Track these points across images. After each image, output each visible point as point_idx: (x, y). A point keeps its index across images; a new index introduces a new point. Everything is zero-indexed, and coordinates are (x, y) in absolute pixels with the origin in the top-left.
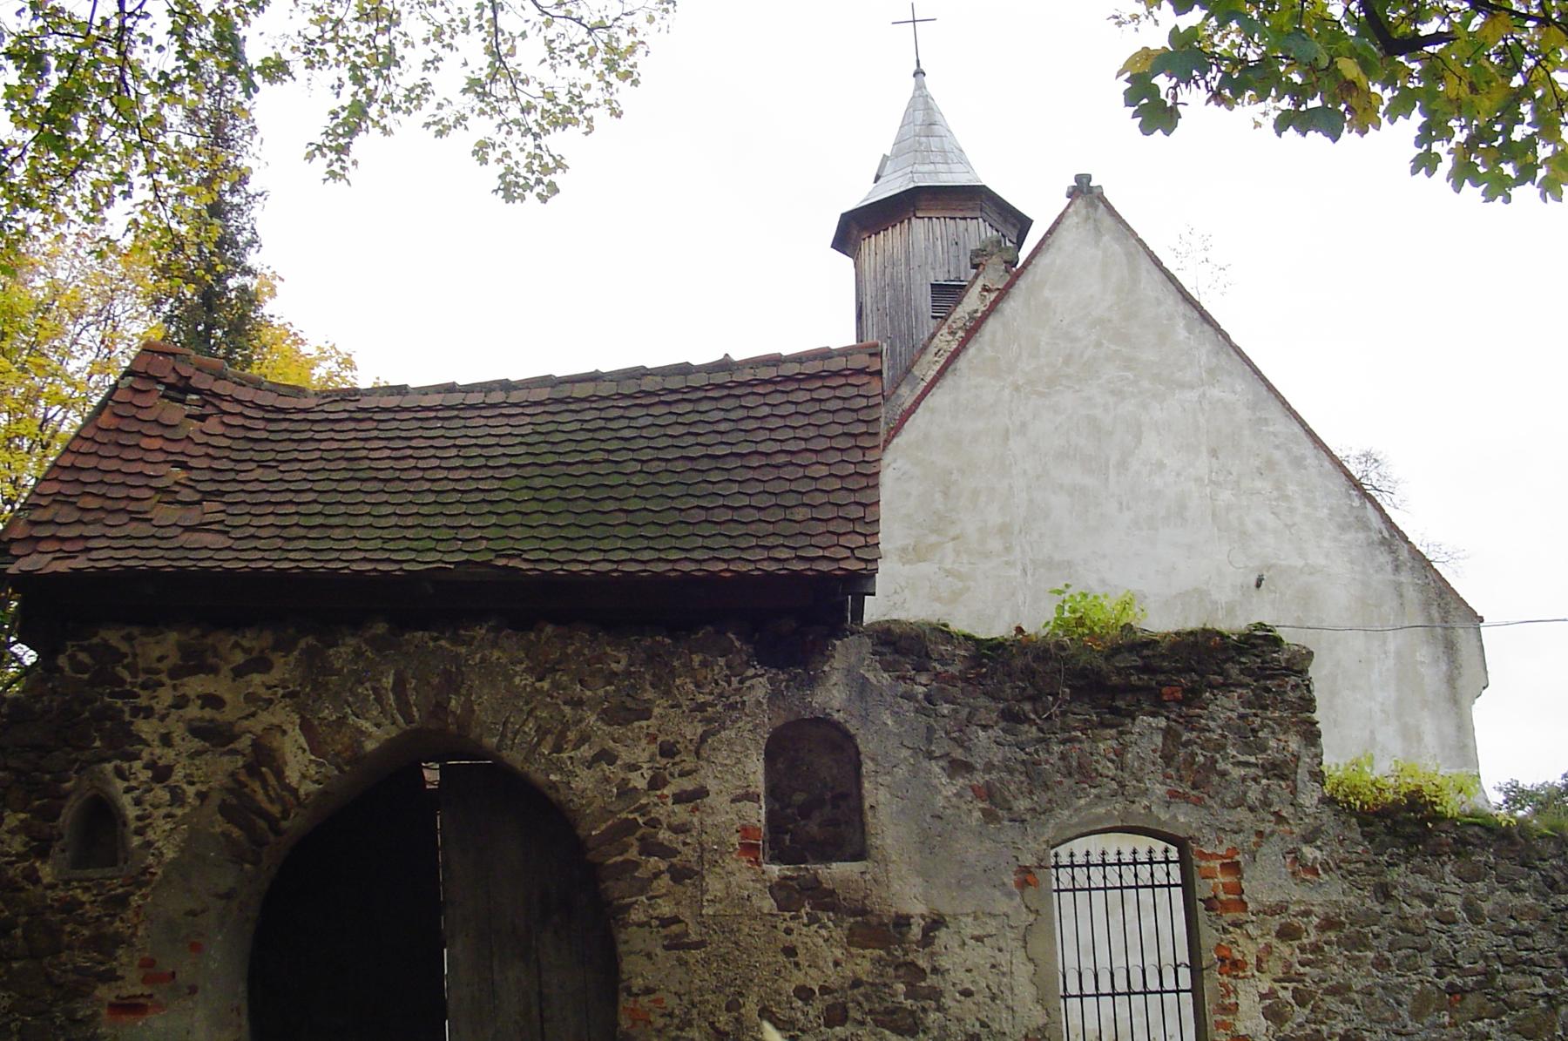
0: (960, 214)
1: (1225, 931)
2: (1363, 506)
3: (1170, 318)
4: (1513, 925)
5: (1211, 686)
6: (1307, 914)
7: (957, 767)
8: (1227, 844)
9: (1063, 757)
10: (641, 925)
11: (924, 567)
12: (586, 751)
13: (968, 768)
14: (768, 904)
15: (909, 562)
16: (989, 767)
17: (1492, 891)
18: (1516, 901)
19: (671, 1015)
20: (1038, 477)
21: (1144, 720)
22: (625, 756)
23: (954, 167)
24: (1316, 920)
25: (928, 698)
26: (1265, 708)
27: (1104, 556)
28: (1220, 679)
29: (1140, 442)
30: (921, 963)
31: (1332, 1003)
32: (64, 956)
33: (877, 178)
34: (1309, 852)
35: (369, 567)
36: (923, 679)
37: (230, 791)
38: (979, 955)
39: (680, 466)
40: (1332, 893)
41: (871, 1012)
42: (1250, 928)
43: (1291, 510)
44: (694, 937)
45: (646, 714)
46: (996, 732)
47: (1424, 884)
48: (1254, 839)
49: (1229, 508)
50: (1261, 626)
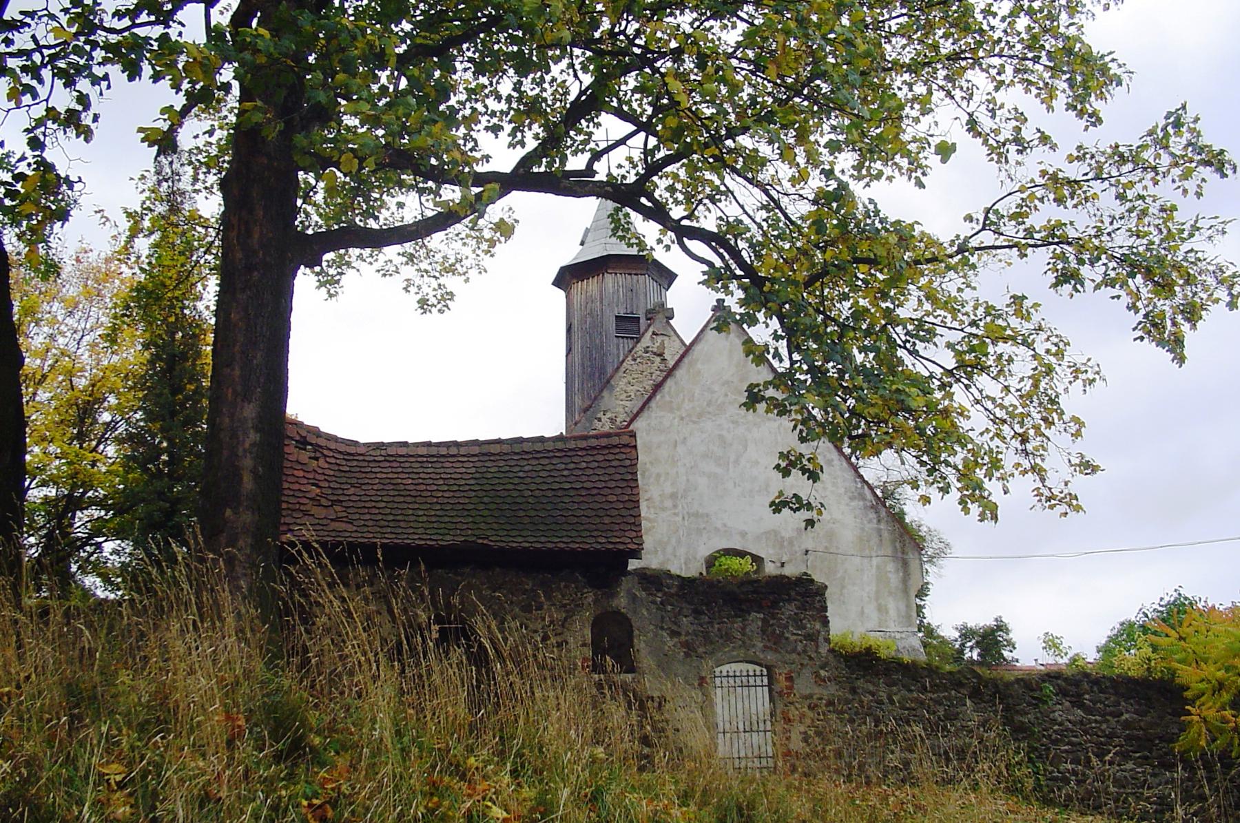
5: (783, 601)
6: (821, 699)
7: (674, 634)
9: (719, 630)
13: (678, 634)
16: (688, 634)
18: (909, 695)
25: (662, 603)
33: (582, 244)
34: (823, 673)
39: (550, 494)
46: (690, 619)
50: (805, 574)
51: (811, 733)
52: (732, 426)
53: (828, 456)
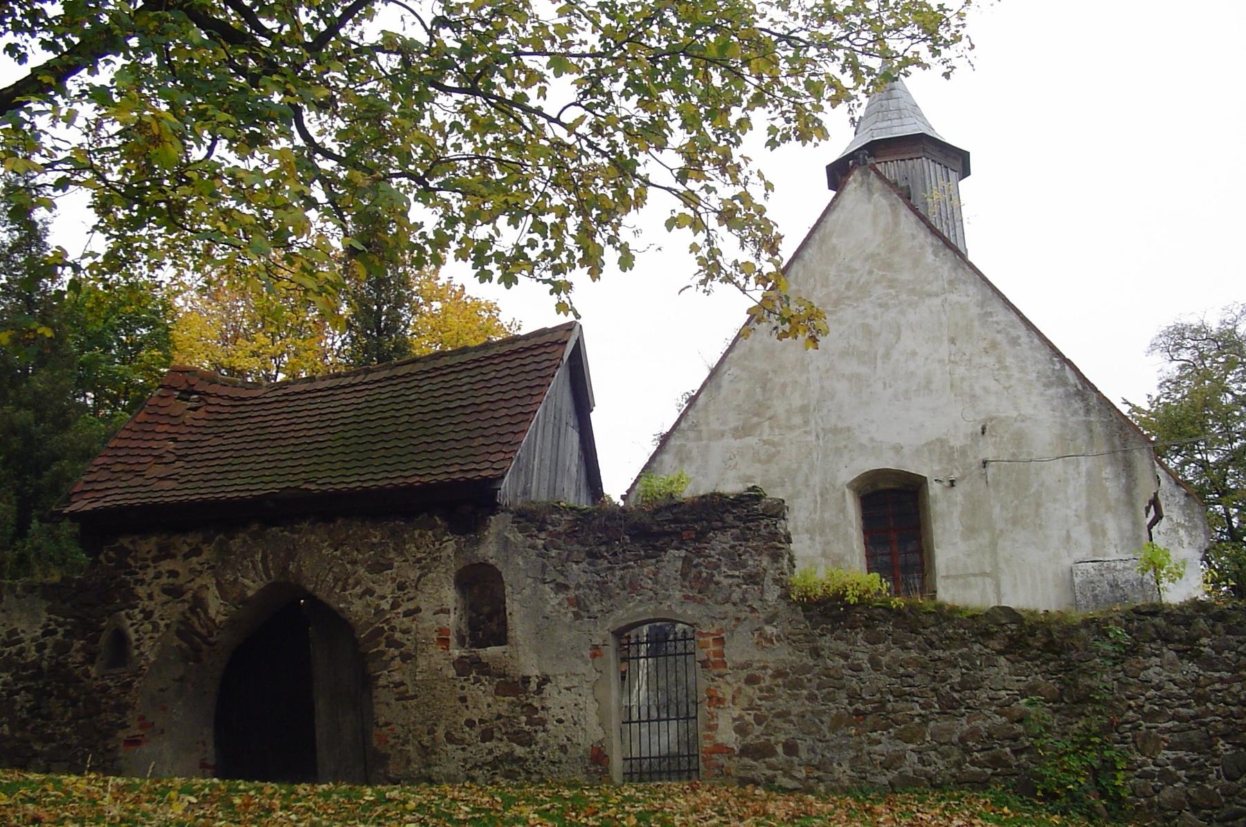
0: (907, 157)
1: (713, 680)
2: (1063, 368)
3: (922, 247)
4: (902, 671)
6: (765, 668)
7: (561, 587)
8: (717, 627)
9: (622, 578)
10: (384, 687)
11: (752, 440)
12: (358, 590)
13: (566, 587)
14: (452, 673)
15: (740, 437)
16: (578, 586)
17: (889, 649)
18: (904, 655)
19: (398, 737)
20: (827, 371)
21: (673, 552)
22: (379, 591)
23: (906, 121)
24: (770, 672)
25: (545, 548)
26: (747, 540)
27: (873, 422)
28: (719, 524)
29: (899, 339)
30: (535, 704)
31: (778, 723)
32: (103, 715)
35: (236, 494)
36: (543, 535)
37: (181, 622)
38: (568, 698)
40: (783, 654)
41: (506, 733)
42: (728, 678)
43: (1009, 377)
44: (411, 693)
45: (390, 567)
46: (584, 565)
47: (842, 646)
48: (734, 622)
49: (963, 379)
51: (749, 718)
52: (879, 310)
53: (1014, 333)
